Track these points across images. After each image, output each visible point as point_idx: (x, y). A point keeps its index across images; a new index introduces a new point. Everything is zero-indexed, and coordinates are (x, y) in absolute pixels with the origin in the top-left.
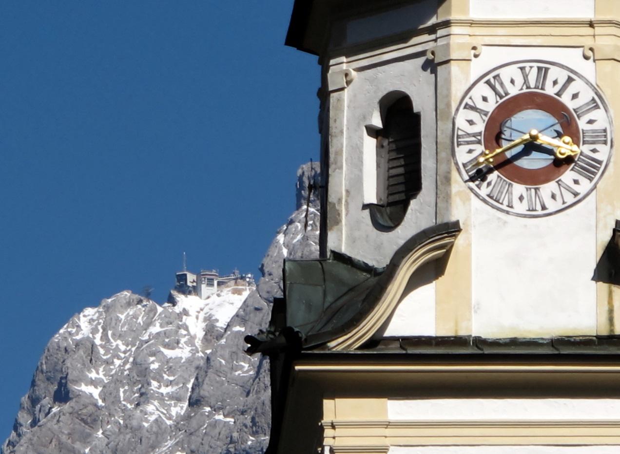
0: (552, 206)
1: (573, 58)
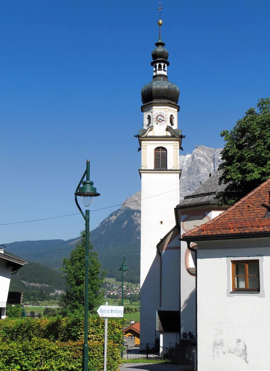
0: (162, 124)
1: (164, 112)
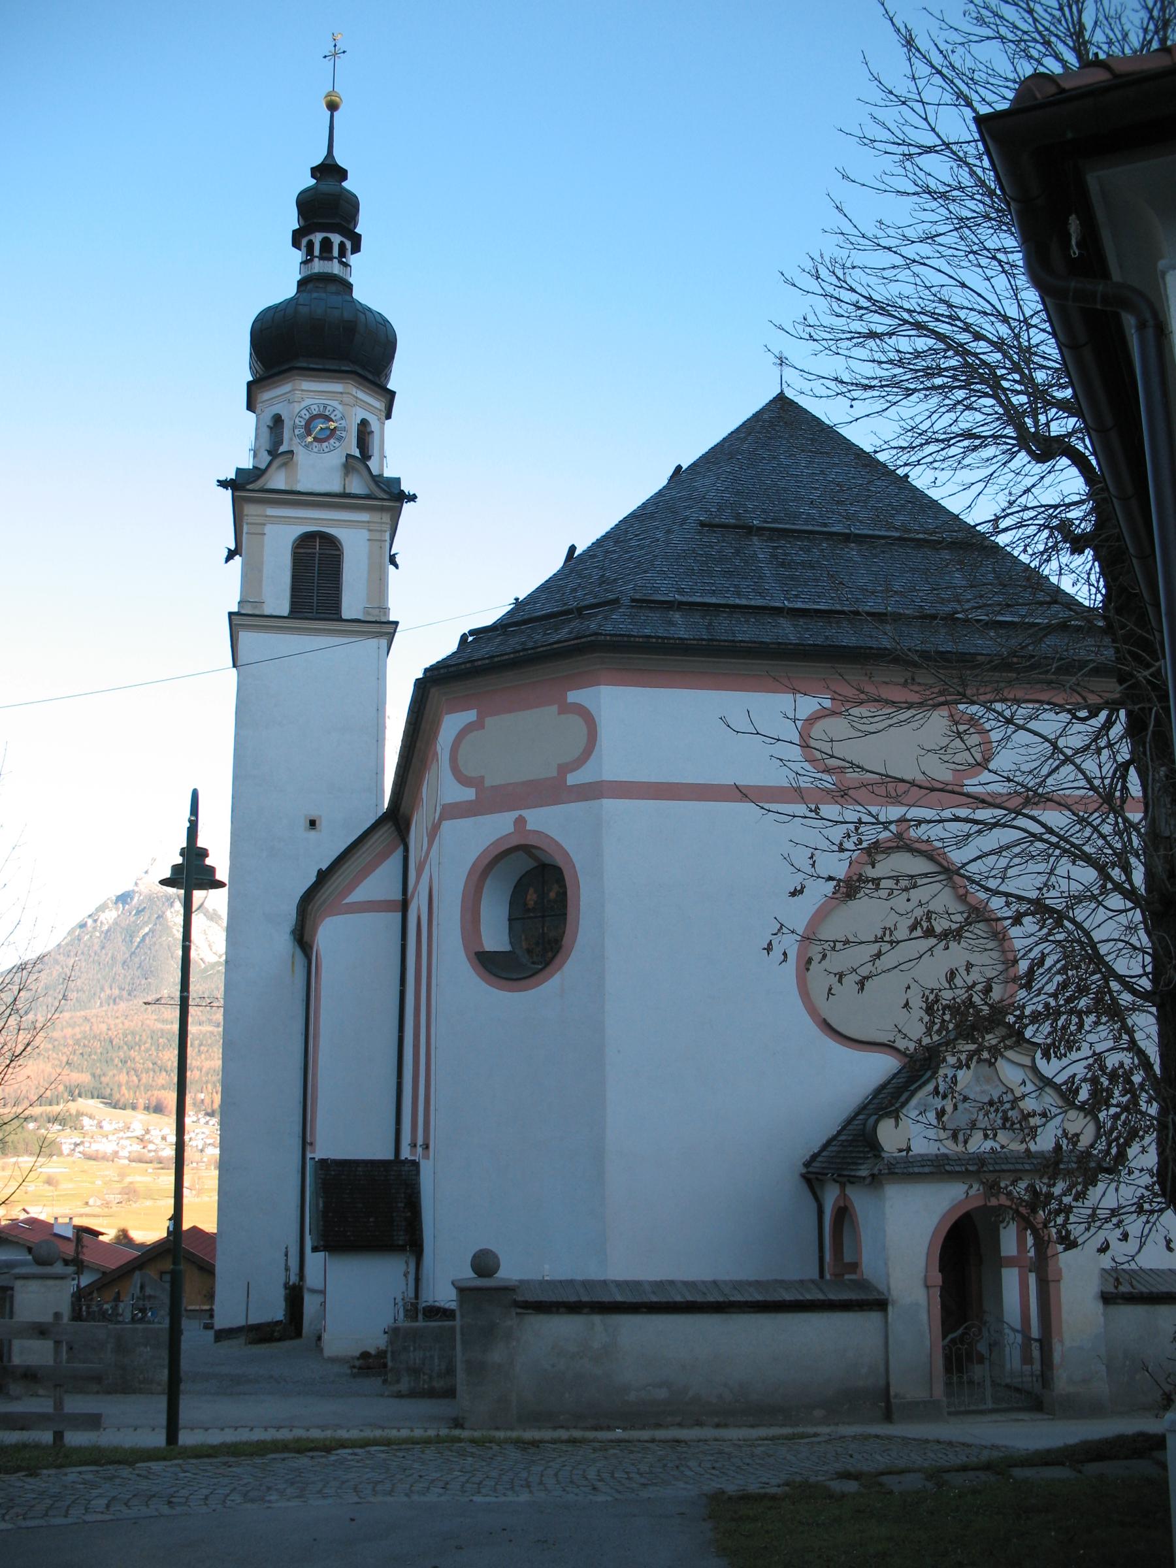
0: (326, 450)
